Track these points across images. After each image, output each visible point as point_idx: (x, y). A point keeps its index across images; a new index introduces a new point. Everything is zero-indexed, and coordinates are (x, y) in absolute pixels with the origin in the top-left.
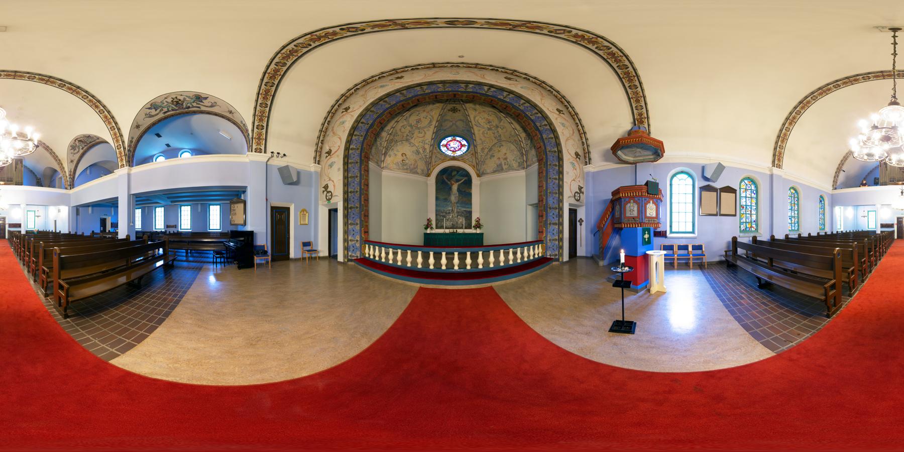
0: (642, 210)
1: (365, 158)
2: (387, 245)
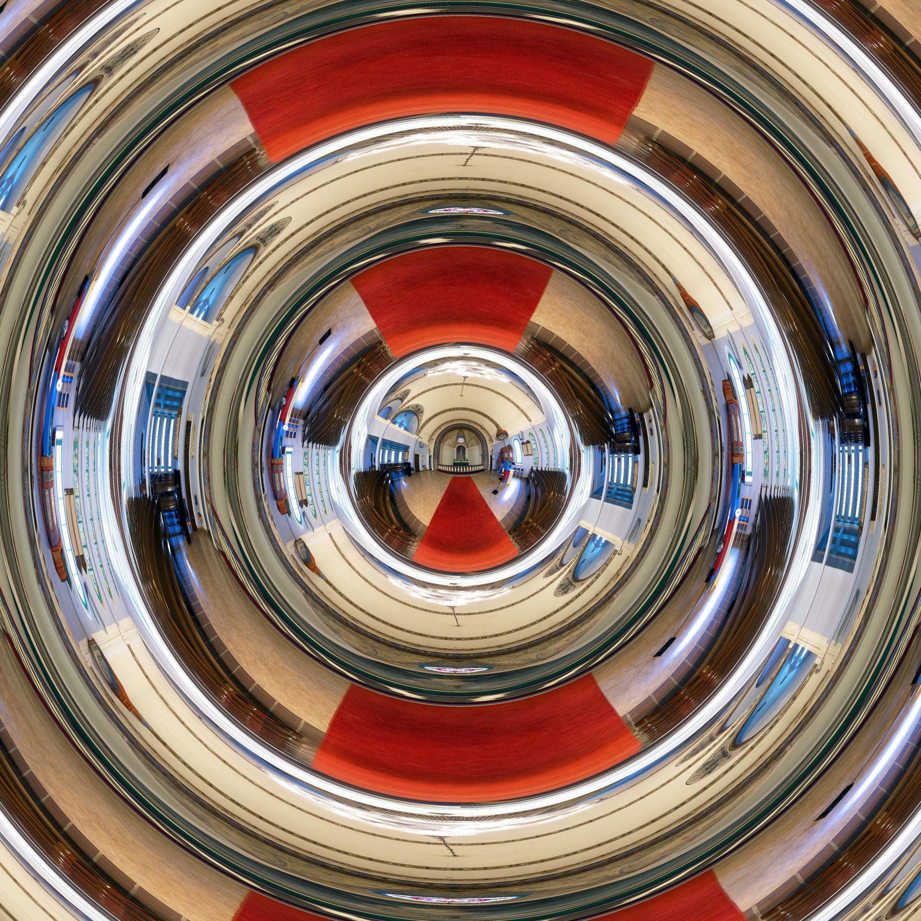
0: (509, 455)
1: (440, 442)
2: (444, 466)
